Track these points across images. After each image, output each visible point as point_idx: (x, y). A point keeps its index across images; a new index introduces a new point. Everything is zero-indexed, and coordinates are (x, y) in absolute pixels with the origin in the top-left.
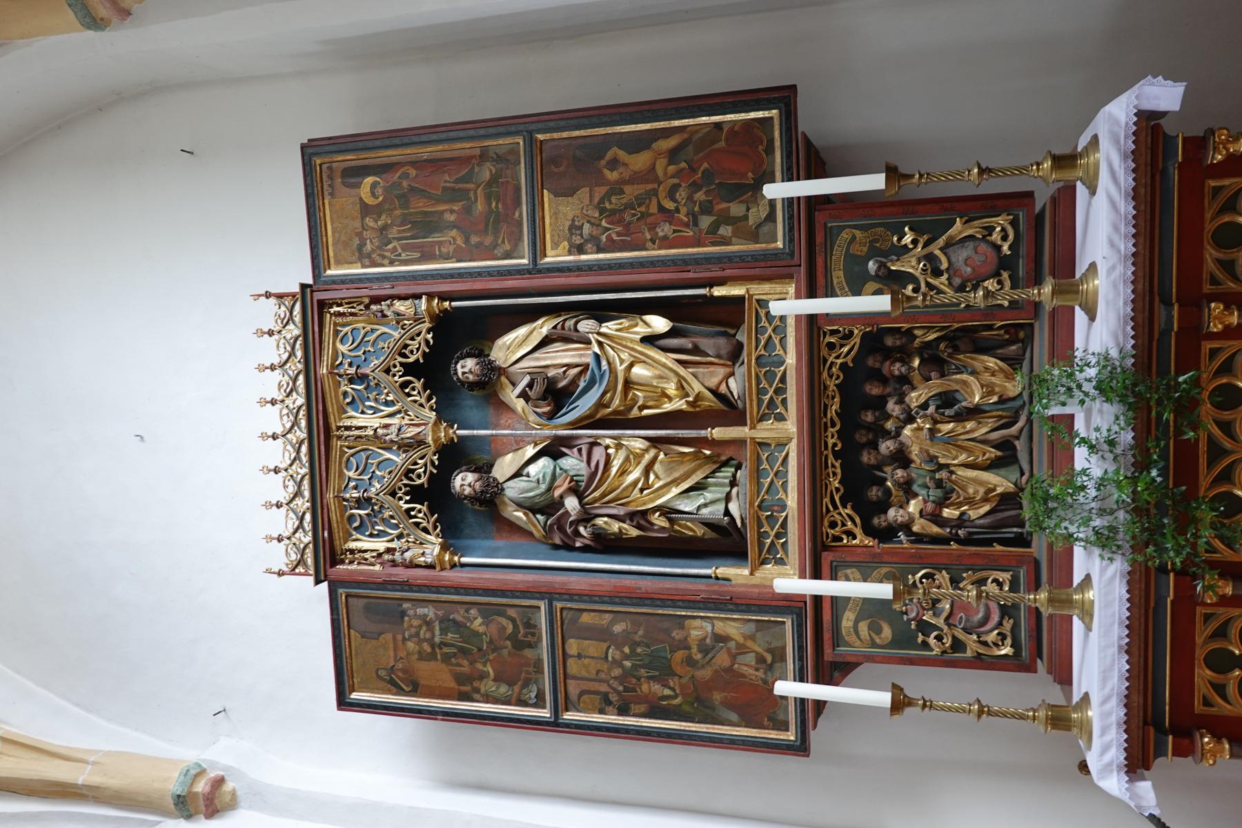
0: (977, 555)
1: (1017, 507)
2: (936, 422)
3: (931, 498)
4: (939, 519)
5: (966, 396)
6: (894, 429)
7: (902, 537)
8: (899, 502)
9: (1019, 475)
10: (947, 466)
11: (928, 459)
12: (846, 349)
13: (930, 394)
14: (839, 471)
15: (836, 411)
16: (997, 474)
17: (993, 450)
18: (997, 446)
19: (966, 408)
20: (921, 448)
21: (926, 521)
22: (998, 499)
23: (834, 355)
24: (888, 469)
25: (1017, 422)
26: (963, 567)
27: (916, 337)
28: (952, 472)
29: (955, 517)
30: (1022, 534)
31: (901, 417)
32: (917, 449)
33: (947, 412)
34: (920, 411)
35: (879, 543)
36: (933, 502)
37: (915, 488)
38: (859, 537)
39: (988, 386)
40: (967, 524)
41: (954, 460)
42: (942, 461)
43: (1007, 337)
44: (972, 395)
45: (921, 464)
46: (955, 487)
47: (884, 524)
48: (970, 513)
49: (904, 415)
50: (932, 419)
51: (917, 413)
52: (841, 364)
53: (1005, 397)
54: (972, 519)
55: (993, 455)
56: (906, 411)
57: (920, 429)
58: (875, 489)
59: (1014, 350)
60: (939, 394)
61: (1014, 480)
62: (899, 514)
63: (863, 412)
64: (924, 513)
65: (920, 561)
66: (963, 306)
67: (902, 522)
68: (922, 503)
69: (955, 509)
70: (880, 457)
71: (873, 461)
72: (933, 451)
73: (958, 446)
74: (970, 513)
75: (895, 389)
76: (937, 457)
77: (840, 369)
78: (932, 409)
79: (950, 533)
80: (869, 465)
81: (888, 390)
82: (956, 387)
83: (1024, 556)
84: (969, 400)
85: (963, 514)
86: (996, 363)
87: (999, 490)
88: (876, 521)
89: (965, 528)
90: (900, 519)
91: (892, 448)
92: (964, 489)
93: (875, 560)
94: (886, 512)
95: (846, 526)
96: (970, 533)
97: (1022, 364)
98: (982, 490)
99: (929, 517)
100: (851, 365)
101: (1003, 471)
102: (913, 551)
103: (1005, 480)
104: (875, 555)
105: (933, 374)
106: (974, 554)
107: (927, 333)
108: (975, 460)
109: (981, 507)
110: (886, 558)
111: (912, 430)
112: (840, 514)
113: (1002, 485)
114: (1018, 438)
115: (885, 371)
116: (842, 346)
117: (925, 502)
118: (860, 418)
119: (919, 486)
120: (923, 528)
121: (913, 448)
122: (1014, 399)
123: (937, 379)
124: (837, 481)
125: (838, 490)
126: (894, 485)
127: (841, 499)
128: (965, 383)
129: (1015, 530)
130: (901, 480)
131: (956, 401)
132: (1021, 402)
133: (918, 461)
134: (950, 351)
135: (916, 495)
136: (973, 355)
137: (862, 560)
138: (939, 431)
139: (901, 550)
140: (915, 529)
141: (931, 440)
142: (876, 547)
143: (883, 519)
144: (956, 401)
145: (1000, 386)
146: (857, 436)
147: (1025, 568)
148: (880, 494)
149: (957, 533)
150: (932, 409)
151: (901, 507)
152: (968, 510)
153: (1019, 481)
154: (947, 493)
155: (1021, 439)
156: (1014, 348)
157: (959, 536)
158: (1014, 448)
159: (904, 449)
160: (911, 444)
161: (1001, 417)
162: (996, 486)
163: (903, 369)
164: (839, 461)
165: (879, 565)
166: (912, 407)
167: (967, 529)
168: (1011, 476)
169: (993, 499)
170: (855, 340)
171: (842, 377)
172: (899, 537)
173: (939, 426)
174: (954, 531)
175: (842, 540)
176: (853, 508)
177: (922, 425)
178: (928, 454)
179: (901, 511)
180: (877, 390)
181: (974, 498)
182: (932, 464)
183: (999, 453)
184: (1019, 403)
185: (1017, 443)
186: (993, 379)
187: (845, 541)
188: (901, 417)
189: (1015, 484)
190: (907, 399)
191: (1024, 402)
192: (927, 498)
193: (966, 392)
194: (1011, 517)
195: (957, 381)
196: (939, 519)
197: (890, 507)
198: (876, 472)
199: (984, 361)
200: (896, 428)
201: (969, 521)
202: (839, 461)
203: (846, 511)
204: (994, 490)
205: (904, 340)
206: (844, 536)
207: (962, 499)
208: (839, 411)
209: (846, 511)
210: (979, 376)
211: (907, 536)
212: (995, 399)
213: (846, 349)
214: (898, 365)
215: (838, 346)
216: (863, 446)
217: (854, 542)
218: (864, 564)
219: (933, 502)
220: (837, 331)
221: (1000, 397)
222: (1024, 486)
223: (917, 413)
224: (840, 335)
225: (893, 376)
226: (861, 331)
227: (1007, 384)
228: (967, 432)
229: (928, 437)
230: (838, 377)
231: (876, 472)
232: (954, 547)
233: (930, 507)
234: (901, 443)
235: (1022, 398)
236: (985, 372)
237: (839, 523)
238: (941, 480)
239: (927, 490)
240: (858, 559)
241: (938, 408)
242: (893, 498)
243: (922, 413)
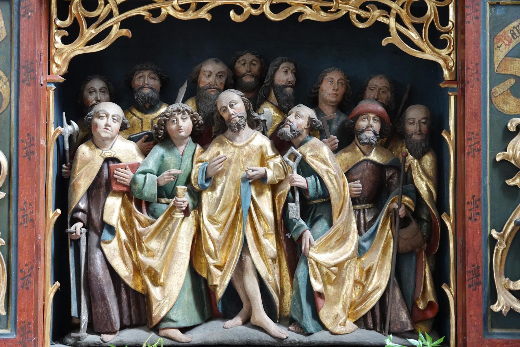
0: (37, 252)
1: (126, 321)
2: (275, 188)
3: (140, 178)
4: (103, 190)
5: (323, 238)
6: (262, 117)
7: (70, 128)
8: (133, 126)
9: (183, 324)
10: (198, 206)
11: (210, 173)
12: (413, 35)
13: (326, 179)
14: (189, 16)
15: (301, 13)
16: (183, 289)
17: (227, 282)
18: (231, 288)
19: (301, 238)
20: (230, 162)
21: (97, 169)
22: (139, 289)
23: (403, 13)
24: (190, 106)
25: (274, 320)
26: (13, 228)
27: (419, 158)
28: (186, 212)
29: (105, 218)
30: (77, 327)
31: (286, 130)
32: (229, 156)
33: (294, 209)
34: (298, 160)
35: (56, 84)
36: (134, 181)
37: (158, 151)
38: (68, 48)
39: (338, 275)
40: (94, 238)
41: (210, 217)
42: (207, 197)
43: (421, 306)
44: (326, 248)
45: (201, 161)
46: (160, 219)
47: (92, 98)
48: (115, 243)
49: (290, 135)
50: (281, 182)
51: (294, 157)
52: (386, 27)
53: (320, 301)
54: (103, 245)
55: (217, 282)
56: (296, 137)
57: (263, 161)
58: (155, 83)
59: (398, 316)
60: (326, 195)
61: (173, 317)
62: (110, 122)
63: (292, 66)
64: (112, 164)
65: (22, 153)
66: (495, 234)
67: (96, 126)
68: (132, 161)
69: (120, 218)
70: (212, 93)
71: (205, 81)
72: (221, 183)
73: (233, 225)
74: (115, 243)
75: (330, 122)
76: (213, 188)
77: (377, 23)
78: (300, 181)
79: (78, 210)
80: (198, 73)
81: (329, 111)
82: (338, 222)
83: (36, 334)
84: (315, 243)
85: (112, 230)
86: (378, 288)
87: (155, 292)
88: (97, 84)
89: (87, 235)
90: (101, 123)
91: (231, 111)
92: (159, 233)
93: (23, 71)
94: (113, 99)
95: (88, 26)
96: (77, 243)
97: (374, 329)
98: (153, 262)
99: (106, 173)
100: (384, 43)
101: (189, 298)
102: (43, 143)
103: (173, 300)
104: (32, 70)
105: (358, 184)
106: (38, 249)
107: (428, 176)
108: (209, 253)
109: (124, 262)
110: (27, 91)
111: (261, 147)
112: (111, 15)
113: (164, 297)
114: (247, 322)
115: (365, 105)
116: (418, 28)
117: (134, 167)
118: (282, 62)
119: (163, 157)
120: (86, 162)
121: (232, 149)
122: (316, 316)
123: (351, 191)
124: (172, 12)
125: (156, 12)
126: (164, 114)
127: (140, 17)
128: (343, 239)
129: (85, 317)
130: (174, 127)
131: (312, 223)
132: (311, 329)
133: (206, 156)
134: (402, 212)
135: (145, 153)
136: (391, 250)
137: (23, 47)
138: (260, 193)
139: (43, 121)
140: (84, 150)
141: (245, 179)
142: (49, 78)
143: (100, 96)
144: (312, 223)
145: (338, 295)
146: (248, 57)
147: (413, 210)
148: (146, 91)
149: (78, 220)
150: (300, 181)
151: (123, 127)
152: (119, 240)
153: (172, 324)
154: (148, 204)
155: (244, 328)
156: (404, 316)
157: (72, 224)
158: (227, 316)
159: (229, 133)
160: (239, 144)
161: (281, 294)
162: (163, 286)
163: (369, 134)
164: (208, 17)
165: (14, 78)
166: (302, 148)
167: (84, 237)
168: (180, 312)
169: (139, 282)
170: (428, 50)
171: (361, 26)
172: (69, 123)
173: (268, 193)
174: (80, 215)
175: (62, 16)
176: (121, 40)
177: (271, 165)
178: (218, 174)
179: (116, 126)
180: (330, 91)
181: (142, 251)
182: (201, 180)
183: (220, 292)
184: (309, 324)
185: (238, 320)
186: (349, 283)
187: (59, 22)
188: (286, 130)
189: (165, 319)
190: (315, 140)
191: (311, 334)
192: (140, 169)
193: (330, 238)
194: (108, 311)
195: (347, 224)
196: (103, 190)
197: (123, 109)
198: (185, 87)
199: (381, 268)
200: (265, 121)
201: (100, 241)
202: (208, 17)
203: (116, 28)
204: (155, 283)
205: (417, 138)
206: (68, 22)
207: (140, 229)
208: (301, 19)
209: (116, 28)
210: (355, 259)
211: (71, 137)
212: (317, 286)
213: (413, 35)
214: (376, 126)
215: (418, 20)
216: (231, 67)
217: (58, 39)
218: (15, 51)
219: (134, 181)
220: (445, 20)
221: (320, 295)
222: (162, 332)
223: (294, 157)
224: (438, 26)
225: (356, 118)
226: (445, 60)
227: (341, 306)
228: (257, 239)
229: (250, 173)
230: (362, 20)
231: (185, 87)
232: (51, 214)
233: (126, 175)
234: (239, 127)
235: (318, 331)
236: (362, 269)
237: (95, 14)
238: (173, 194)
239: (155, 171)
240: (24, 40)
241: (303, 191)
242: (139, 114)
243: (293, 164)
